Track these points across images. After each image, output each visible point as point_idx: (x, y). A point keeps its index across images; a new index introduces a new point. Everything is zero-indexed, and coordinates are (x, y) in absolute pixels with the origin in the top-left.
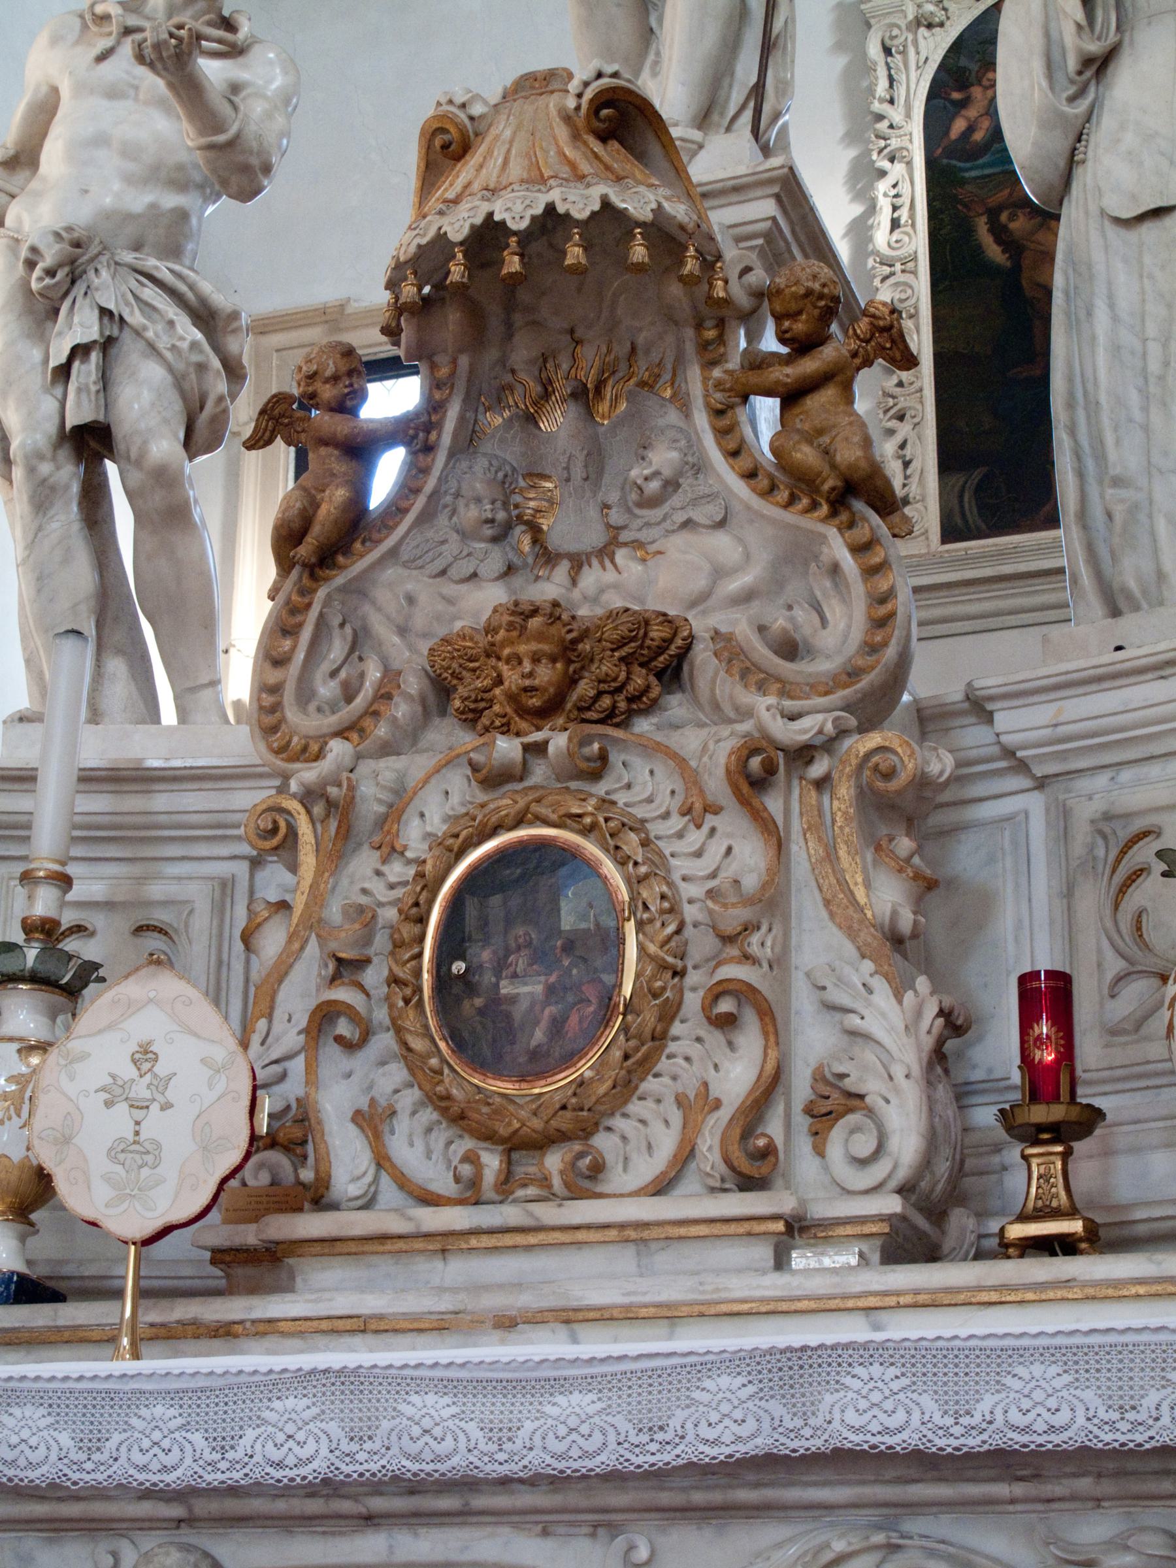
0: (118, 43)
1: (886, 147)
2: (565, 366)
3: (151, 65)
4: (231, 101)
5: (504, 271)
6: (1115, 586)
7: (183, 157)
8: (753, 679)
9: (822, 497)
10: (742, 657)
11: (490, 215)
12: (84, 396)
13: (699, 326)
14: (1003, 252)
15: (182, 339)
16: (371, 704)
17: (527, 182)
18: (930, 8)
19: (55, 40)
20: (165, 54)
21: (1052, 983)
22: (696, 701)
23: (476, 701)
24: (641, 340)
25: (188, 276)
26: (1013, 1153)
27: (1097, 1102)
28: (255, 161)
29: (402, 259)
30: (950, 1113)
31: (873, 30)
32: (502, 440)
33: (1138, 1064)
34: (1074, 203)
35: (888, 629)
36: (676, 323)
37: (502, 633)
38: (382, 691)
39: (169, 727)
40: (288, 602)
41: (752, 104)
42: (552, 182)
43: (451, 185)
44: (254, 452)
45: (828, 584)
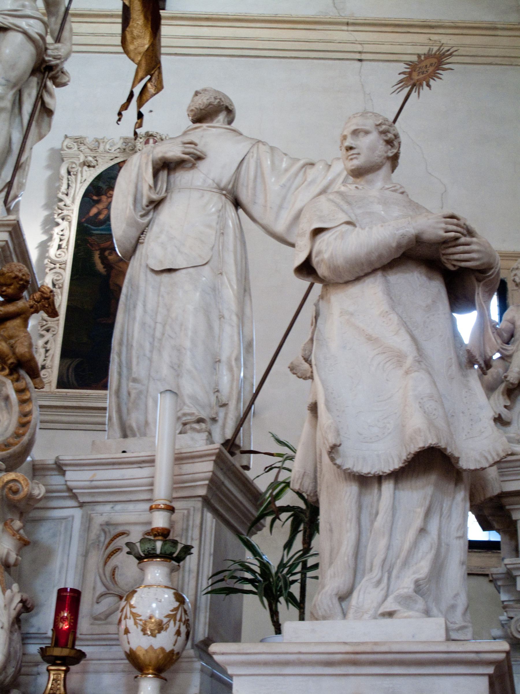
9: (7, 365)
14: (104, 268)
18: (90, 159)
21: (72, 594)
26: (44, 667)
27: (84, 649)
30: (18, 646)
31: (64, 163)
33: (104, 634)
41: (6, 190)
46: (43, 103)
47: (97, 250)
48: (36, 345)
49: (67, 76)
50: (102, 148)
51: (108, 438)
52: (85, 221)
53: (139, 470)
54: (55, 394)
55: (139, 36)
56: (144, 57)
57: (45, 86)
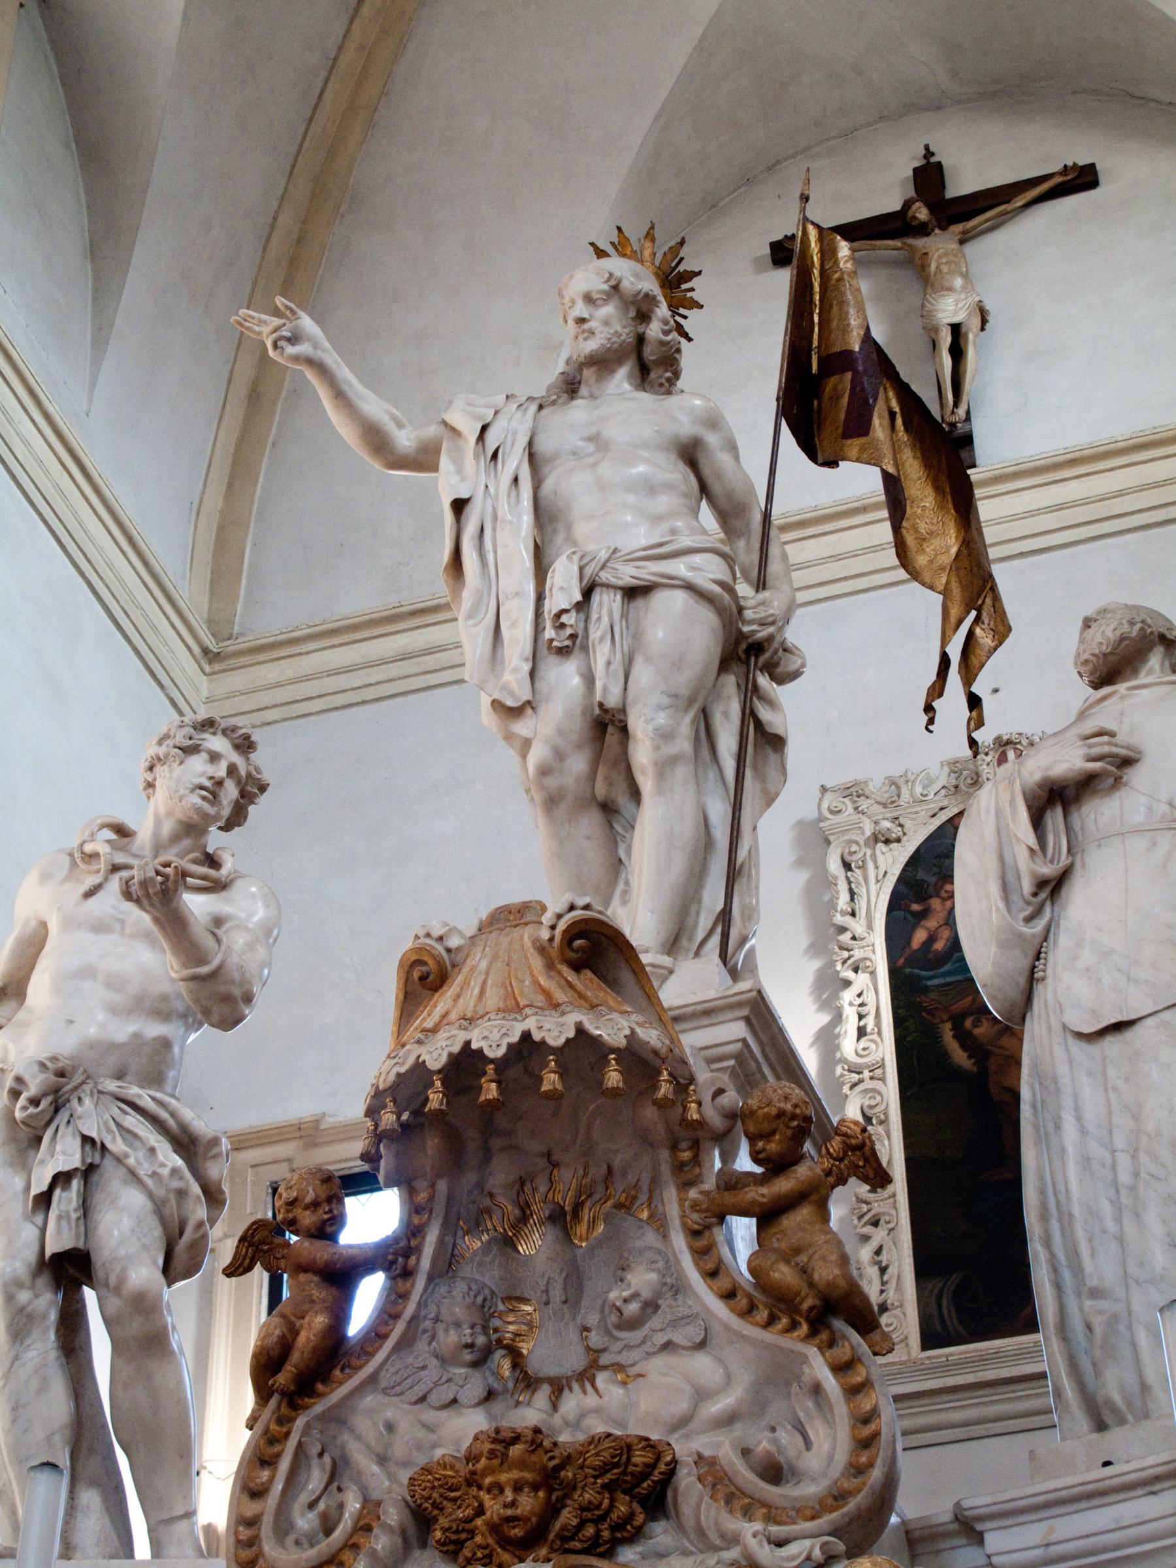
0: (106, 879)
1: (849, 958)
2: (543, 1189)
3: (138, 901)
4: (214, 934)
5: (482, 1098)
6: (1100, 1399)
7: (166, 988)
8: (738, 1504)
9: (801, 1315)
10: (727, 1482)
11: (468, 1043)
12: (64, 1223)
13: (674, 1148)
14: (969, 1057)
15: (163, 1165)
16: (351, 1535)
17: (504, 1011)
18: (887, 824)
19: (45, 877)
20: (151, 891)
22: (681, 1528)
23: (457, 1532)
24: (617, 1162)
25: (169, 1103)
28: (237, 992)
29: (381, 1087)
31: (832, 846)
32: (481, 1264)
34: (1036, 1020)
35: (873, 1450)
36: (652, 1145)
37: (483, 1461)
38: (362, 1523)
39: (143, 1562)
40: (266, 1431)
41: (719, 930)
42: (528, 1011)
43: (429, 1015)
44: (234, 1279)
45: (810, 1404)
46: (759, 724)
47: (943, 1022)
48: (858, 1262)
49: (798, 655)
50: (907, 796)
51: (1063, 1439)
52: (904, 963)
53: (1151, 1499)
54: (922, 1364)
55: (932, 533)
56: (953, 573)
57: (756, 688)
